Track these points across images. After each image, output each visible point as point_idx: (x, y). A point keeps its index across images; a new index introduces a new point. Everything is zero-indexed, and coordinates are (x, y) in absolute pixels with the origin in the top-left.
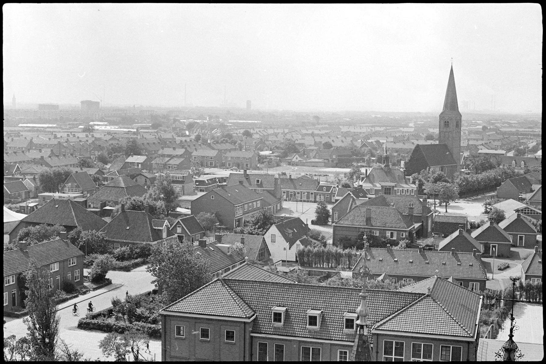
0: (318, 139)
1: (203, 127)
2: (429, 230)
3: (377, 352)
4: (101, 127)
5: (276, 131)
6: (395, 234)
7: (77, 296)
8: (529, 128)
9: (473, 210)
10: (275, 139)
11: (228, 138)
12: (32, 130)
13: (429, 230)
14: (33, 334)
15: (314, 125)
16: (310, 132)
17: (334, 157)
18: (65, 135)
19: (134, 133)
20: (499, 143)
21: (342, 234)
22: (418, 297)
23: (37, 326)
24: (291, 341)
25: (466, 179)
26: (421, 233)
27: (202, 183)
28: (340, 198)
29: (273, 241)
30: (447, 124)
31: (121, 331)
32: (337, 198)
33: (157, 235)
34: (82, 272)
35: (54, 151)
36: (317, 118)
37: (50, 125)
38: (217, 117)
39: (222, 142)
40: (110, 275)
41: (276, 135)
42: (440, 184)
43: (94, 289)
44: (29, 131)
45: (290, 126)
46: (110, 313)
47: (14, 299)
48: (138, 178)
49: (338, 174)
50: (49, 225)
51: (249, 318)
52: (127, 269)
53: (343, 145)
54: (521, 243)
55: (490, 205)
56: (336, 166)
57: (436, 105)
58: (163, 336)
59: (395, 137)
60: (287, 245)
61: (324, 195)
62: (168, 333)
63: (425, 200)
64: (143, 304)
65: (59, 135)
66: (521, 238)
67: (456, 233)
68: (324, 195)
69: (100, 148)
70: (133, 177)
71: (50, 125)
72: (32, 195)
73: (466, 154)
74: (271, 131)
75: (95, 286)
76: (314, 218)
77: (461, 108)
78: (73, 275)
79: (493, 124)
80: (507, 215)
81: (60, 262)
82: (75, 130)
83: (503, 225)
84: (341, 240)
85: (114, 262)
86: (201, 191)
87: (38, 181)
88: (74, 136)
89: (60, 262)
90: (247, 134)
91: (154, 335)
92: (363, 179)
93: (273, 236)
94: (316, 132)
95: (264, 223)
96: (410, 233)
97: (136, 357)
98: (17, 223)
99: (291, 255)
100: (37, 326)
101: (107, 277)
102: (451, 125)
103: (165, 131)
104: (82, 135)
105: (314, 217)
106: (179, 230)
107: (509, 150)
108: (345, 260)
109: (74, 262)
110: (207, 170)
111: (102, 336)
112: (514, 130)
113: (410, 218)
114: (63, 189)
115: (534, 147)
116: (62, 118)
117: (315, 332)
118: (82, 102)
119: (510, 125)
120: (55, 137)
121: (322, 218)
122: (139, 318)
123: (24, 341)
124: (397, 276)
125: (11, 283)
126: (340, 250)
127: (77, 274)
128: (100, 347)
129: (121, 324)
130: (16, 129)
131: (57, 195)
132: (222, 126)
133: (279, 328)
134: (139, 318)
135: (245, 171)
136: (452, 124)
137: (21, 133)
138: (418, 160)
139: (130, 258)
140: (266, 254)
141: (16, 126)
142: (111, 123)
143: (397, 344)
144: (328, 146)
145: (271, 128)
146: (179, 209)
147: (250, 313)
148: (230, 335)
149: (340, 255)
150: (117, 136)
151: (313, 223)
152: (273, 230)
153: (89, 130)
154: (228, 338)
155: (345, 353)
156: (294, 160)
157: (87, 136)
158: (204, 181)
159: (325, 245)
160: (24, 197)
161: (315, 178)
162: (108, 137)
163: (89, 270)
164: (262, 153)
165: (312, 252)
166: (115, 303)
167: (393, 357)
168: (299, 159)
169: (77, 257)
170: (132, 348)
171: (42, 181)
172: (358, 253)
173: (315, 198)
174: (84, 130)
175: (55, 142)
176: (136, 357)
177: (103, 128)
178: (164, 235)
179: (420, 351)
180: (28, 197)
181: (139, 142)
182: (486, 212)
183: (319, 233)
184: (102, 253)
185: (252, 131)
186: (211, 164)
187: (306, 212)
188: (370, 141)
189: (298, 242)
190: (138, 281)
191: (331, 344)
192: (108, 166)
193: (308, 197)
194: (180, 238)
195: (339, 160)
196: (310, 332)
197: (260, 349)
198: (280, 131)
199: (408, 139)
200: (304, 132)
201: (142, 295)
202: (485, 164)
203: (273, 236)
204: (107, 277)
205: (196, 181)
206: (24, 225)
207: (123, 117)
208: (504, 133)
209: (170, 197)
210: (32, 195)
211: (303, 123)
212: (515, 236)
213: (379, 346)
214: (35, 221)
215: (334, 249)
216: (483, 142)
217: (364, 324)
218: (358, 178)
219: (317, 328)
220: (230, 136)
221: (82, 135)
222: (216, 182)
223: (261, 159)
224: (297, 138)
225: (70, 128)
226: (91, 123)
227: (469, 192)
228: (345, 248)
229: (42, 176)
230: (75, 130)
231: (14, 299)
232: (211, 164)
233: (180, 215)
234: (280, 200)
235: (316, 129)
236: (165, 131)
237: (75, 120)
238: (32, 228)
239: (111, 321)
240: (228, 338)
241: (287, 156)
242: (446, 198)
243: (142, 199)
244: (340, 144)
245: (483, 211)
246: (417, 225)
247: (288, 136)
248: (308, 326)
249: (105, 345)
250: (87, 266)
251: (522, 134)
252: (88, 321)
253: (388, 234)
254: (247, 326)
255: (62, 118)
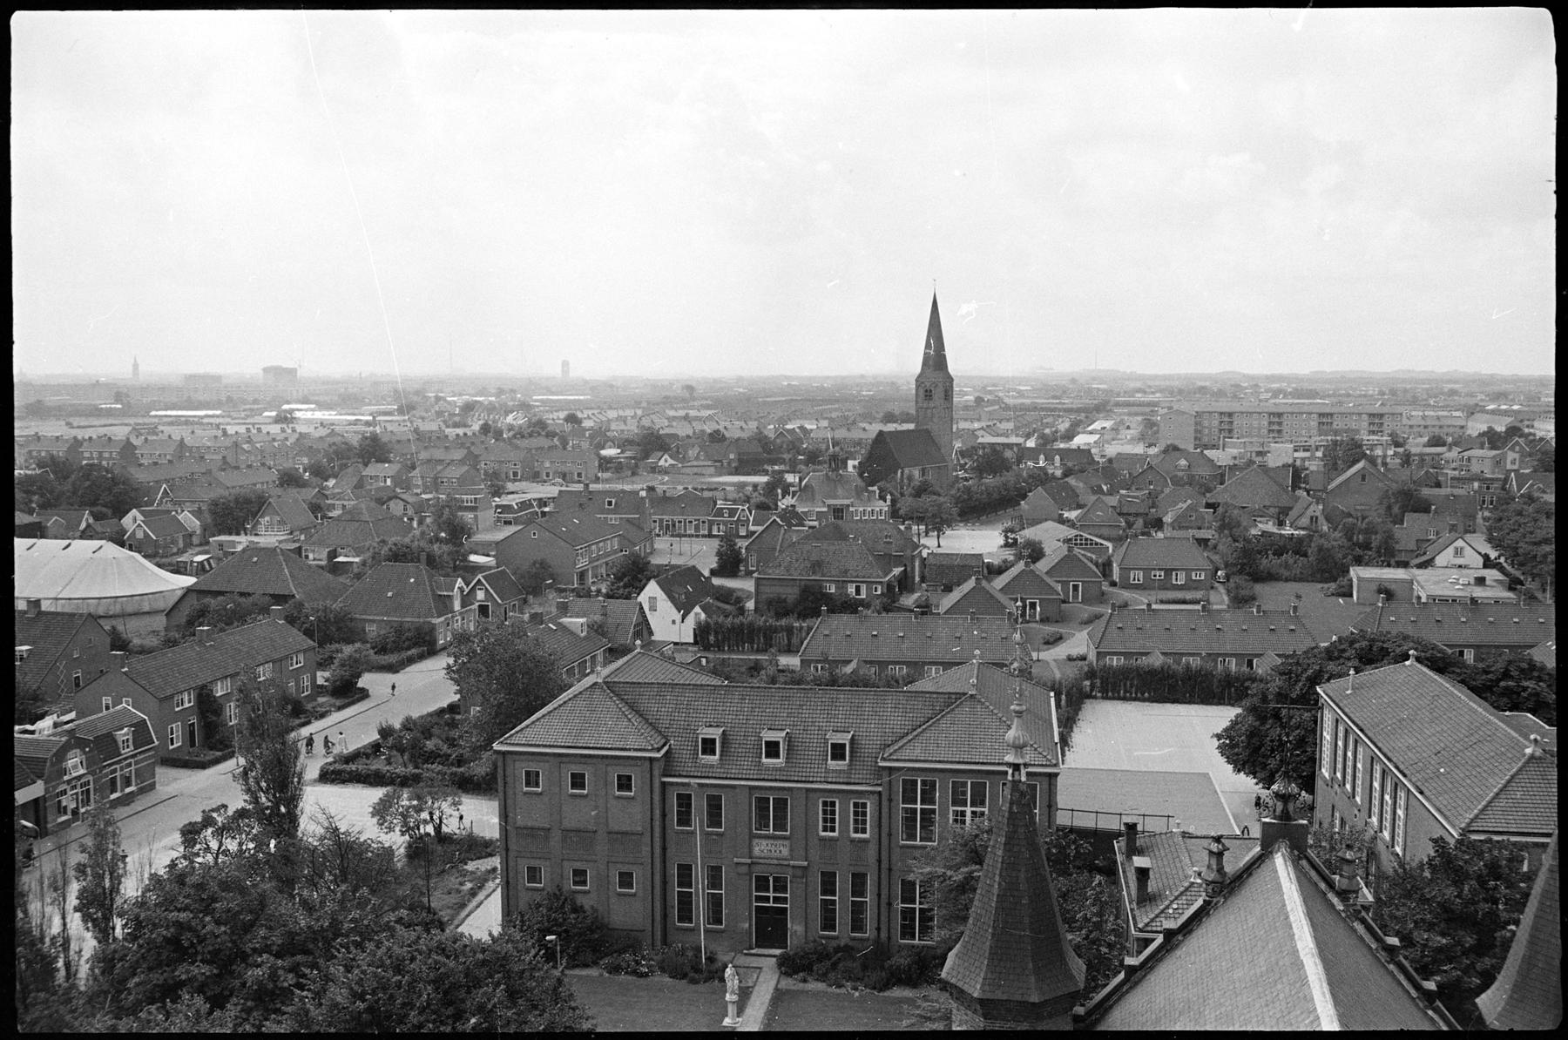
0: (698, 426)
1: (491, 408)
2: (917, 579)
3: (890, 800)
4: (308, 415)
5: (621, 413)
6: (863, 588)
7: (308, 723)
8: (1055, 397)
9: (982, 541)
10: (623, 427)
11: (539, 427)
12: (176, 421)
13: (917, 579)
14: (256, 800)
15: (684, 400)
16: (682, 413)
17: (732, 456)
18: (242, 429)
19: (368, 423)
20: (1010, 425)
21: (770, 591)
22: (953, 700)
23: (264, 784)
24: (733, 787)
25: (968, 489)
26: (905, 583)
27: (506, 508)
28: (760, 529)
29: (653, 609)
30: (928, 395)
31: (405, 782)
32: (752, 528)
33: (444, 604)
34: (314, 679)
35: (229, 459)
36: (690, 388)
37: (210, 413)
38: (513, 391)
39: (531, 435)
40: (366, 681)
41: (624, 420)
42: (926, 499)
43: (340, 708)
44: (171, 424)
45: (644, 404)
46: (376, 748)
47: (192, 734)
48: (392, 504)
49: (742, 486)
50: (242, 594)
51: (659, 750)
52: (393, 669)
53: (745, 435)
54: (1075, 597)
55: (1012, 531)
56: (737, 472)
57: (913, 363)
58: (500, 788)
59: (831, 420)
60: (678, 616)
61: (725, 523)
62: (510, 784)
63: (909, 528)
64: (435, 730)
65: (231, 430)
66: (1076, 588)
67: (971, 583)
68: (725, 523)
69: (310, 451)
70: (380, 502)
71: (210, 413)
72: (196, 540)
73: (958, 445)
74: (612, 414)
75: (338, 703)
76: (714, 565)
77: (952, 368)
78: (297, 684)
79: (990, 392)
80: (1047, 550)
81: (274, 662)
82: (257, 419)
83: (1042, 566)
84: (770, 603)
85: (373, 657)
86: (508, 523)
87: (207, 515)
88: (259, 430)
89: (274, 662)
90: (572, 419)
91: (469, 786)
92: (794, 494)
93: (653, 600)
94: (692, 413)
95: (633, 575)
96: (889, 586)
97: (438, 829)
98: (180, 593)
99: (686, 633)
100: (264, 784)
101: (360, 685)
102: (935, 397)
103: (423, 419)
104: (275, 429)
105: (713, 563)
106: (480, 595)
107: (1028, 436)
108: (782, 638)
109: (298, 662)
110: (510, 486)
111: (376, 794)
112: (1028, 401)
113: (887, 560)
114: (254, 527)
115: (1067, 430)
116: (229, 399)
117: (776, 769)
118: (265, 370)
119: (1021, 394)
120: (225, 433)
121: (730, 564)
122: (432, 757)
123: (242, 813)
124: (879, 663)
125: (187, 705)
126: (772, 622)
127: (306, 680)
128: (373, 815)
129: (400, 770)
130: (147, 420)
131: (242, 541)
132: (524, 406)
133: (712, 766)
134: (432, 757)
135: (587, 486)
136: (938, 394)
137: (161, 428)
138: (881, 460)
139: (397, 648)
140: (645, 633)
141: (147, 415)
142: (322, 406)
143: (924, 783)
144: (717, 437)
145: (611, 408)
146: (473, 558)
147: (659, 741)
148: (625, 783)
149: (775, 630)
150: (337, 429)
151: (713, 573)
152: (652, 589)
153: (284, 419)
154: (620, 788)
155: (833, 804)
156: (662, 463)
157: (283, 430)
158: (510, 507)
159: (742, 611)
160: (181, 545)
161: (707, 494)
162: (323, 432)
163: (327, 674)
164: (604, 452)
165: (722, 626)
166: (385, 732)
167: (919, 806)
168: (671, 461)
169: (305, 651)
170: (431, 814)
171: (213, 513)
172: (796, 625)
173: (710, 530)
174: (278, 420)
175: (228, 442)
176: (438, 829)
177: (309, 415)
178: (457, 606)
179: (965, 793)
180: (189, 545)
181: (385, 439)
182: (1006, 545)
183: (731, 591)
184: (349, 641)
185: (580, 415)
186: (515, 474)
187: (702, 555)
188: (789, 427)
189: (697, 609)
190: (423, 688)
191: (808, 790)
192: (331, 483)
193: (697, 528)
194: (483, 610)
195: (740, 461)
196: (768, 769)
197: (679, 805)
198: (629, 413)
199: (854, 423)
200: (672, 413)
201: (430, 715)
202: (992, 460)
203: (653, 600)
204: (360, 685)
205: (497, 507)
206: (194, 596)
207: (347, 398)
208: (1015, 408)
209: (457, 532)
210: (196, 540)
211: (666, 397)
212: (1065, 584)
213: (894, 789)
214: (215, 588)
215: (761, 621)
216: (984, 424)
217: (1021, 761)
218: (785, 493)
219: (780, 762)
220: (541, 424)
221: (275, 429)
222: (531, 506)
223: (605, 463)
224: (662, 425)
225: (248, 416)
226: (286, 407)
227: (974, 510)
228: (779, 616)
229: (215, 503)
230: (257, 419)
231: (192, 734)
232: (515, 474)
233: (478, 568)
234: (650, 537)
235: (692, 408)
236: (423, 419)
237: (255, 401)
238: (213, 603)
239: (378, 765)
240: (620, 788)
241: (647, 457)
242: (938, 523)
243: (407, 540)
244: (737, 434)
245: (1002, 542)
246: (897, 571)
247: (646, 422)
248: (764, 760)
249: (381, 811)
250: (322, 665)
251: (1043, 409)
252: (338, 767)
253: (851, 590)
254: (656, 765)
255: (229, 399)
